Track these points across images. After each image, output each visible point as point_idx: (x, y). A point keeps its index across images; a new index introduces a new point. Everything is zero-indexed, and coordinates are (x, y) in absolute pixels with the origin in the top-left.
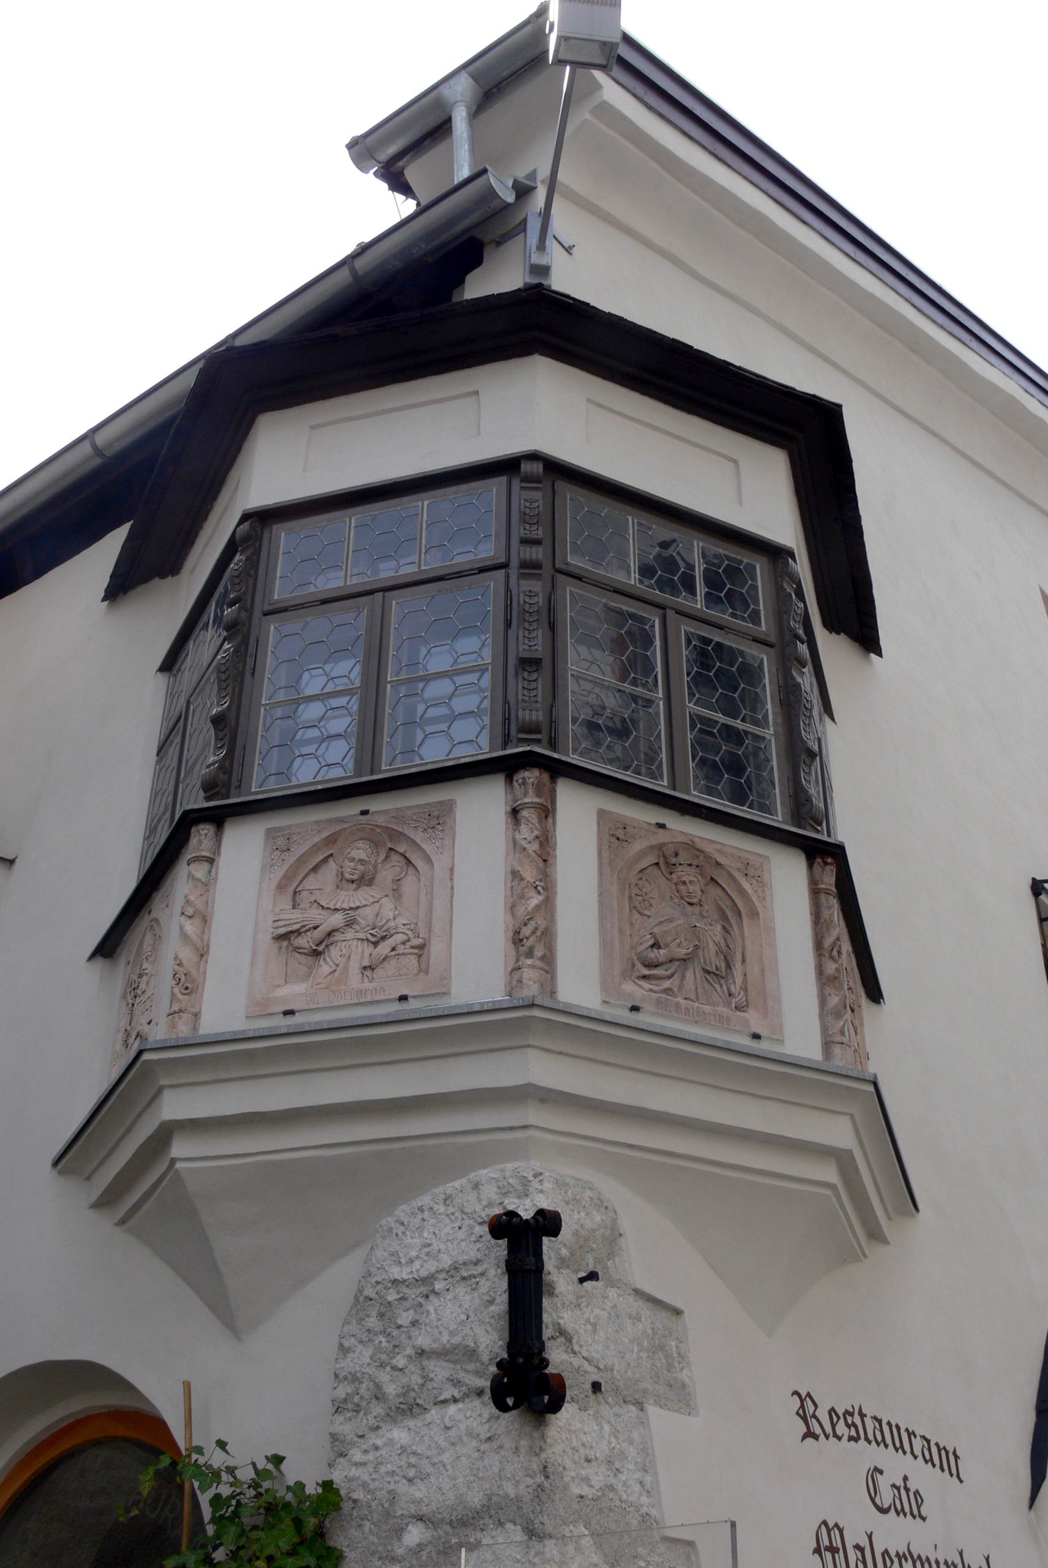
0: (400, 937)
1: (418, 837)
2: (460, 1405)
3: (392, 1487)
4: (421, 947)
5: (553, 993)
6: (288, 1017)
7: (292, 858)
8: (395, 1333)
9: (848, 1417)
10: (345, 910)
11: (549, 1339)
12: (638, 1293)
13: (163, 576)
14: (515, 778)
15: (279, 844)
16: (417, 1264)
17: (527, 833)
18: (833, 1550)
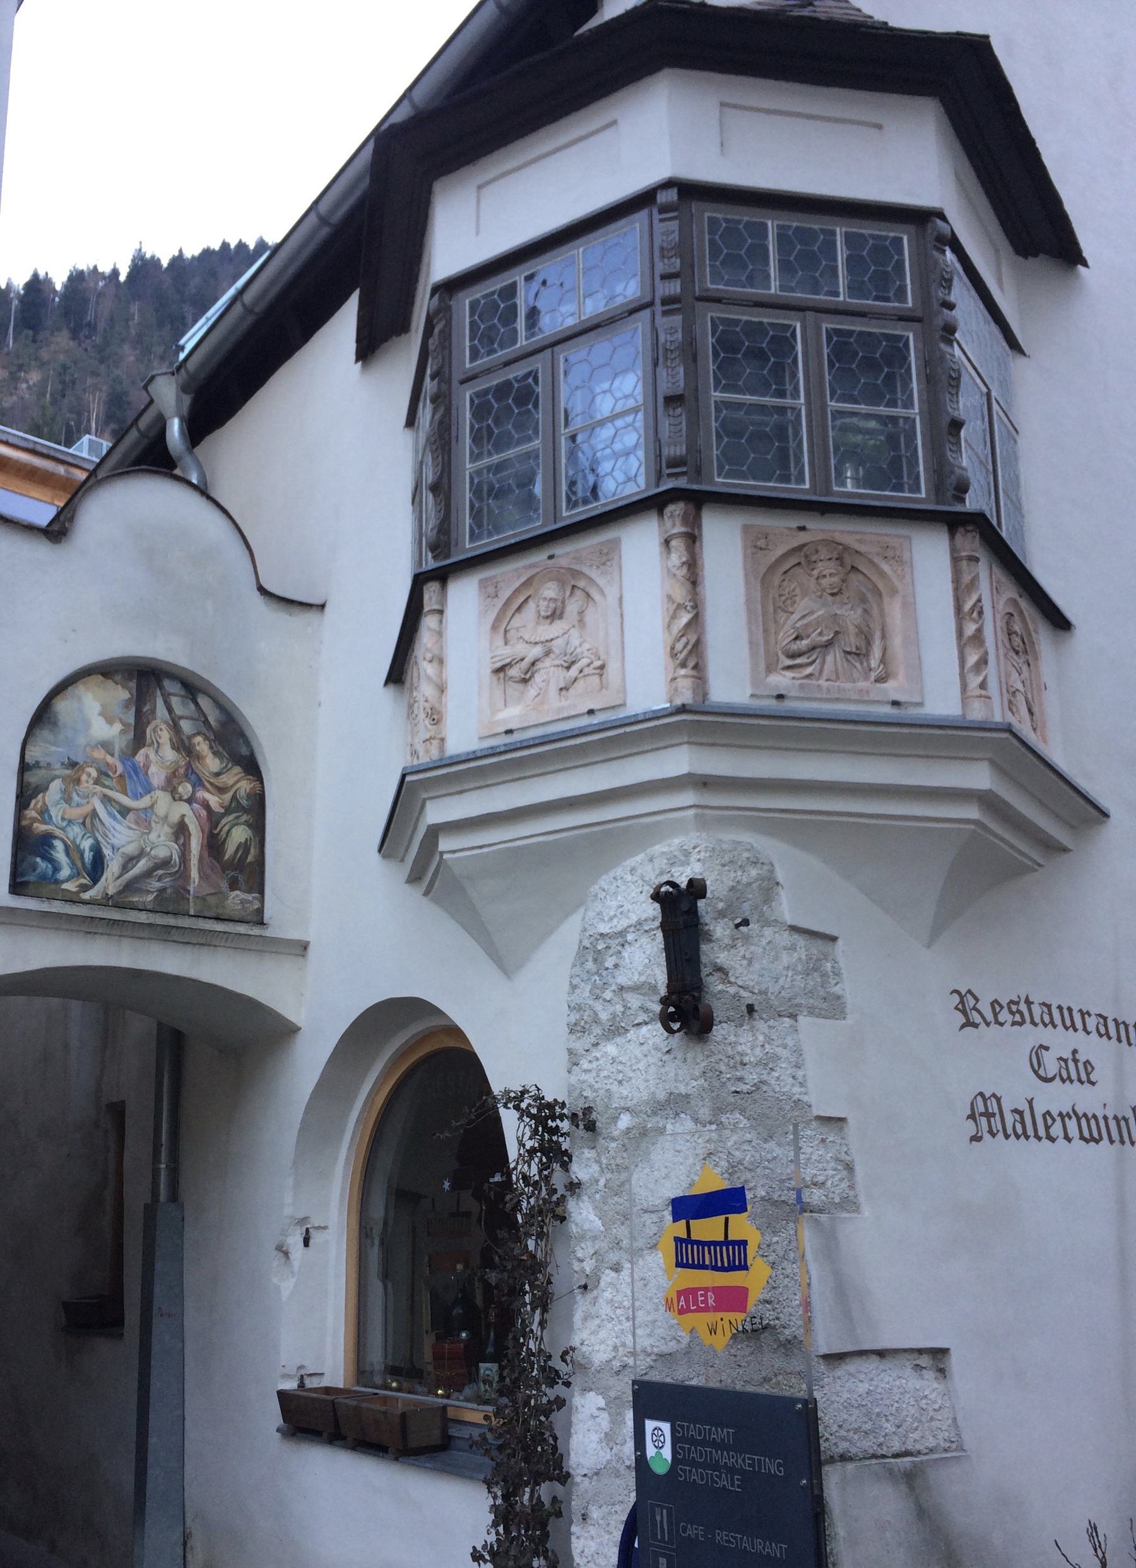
0: (584, 661)
1: (593, 573)
2: (649, 1027)
3: (608, 1087)
4: (602, 667)
5: (705, 695)
6: (509, 735)
7: (499, 603)
8: (604, 973)
9: (1012, 1006)
10: (542, 642)
11: (707, 975)
12: (794, 929)
13: (399, 334)
14: (665, 512)
15: (489, 591)
16: (615, 921)
17: (677, 557)
18: (988, 1115)
